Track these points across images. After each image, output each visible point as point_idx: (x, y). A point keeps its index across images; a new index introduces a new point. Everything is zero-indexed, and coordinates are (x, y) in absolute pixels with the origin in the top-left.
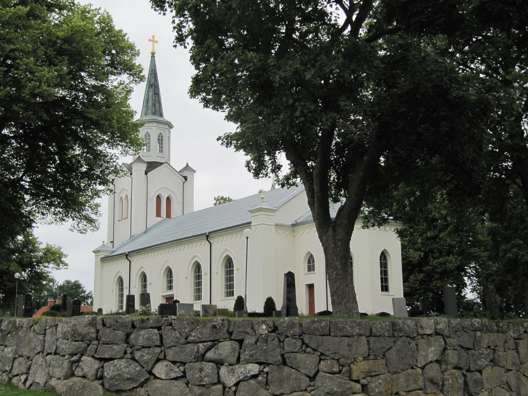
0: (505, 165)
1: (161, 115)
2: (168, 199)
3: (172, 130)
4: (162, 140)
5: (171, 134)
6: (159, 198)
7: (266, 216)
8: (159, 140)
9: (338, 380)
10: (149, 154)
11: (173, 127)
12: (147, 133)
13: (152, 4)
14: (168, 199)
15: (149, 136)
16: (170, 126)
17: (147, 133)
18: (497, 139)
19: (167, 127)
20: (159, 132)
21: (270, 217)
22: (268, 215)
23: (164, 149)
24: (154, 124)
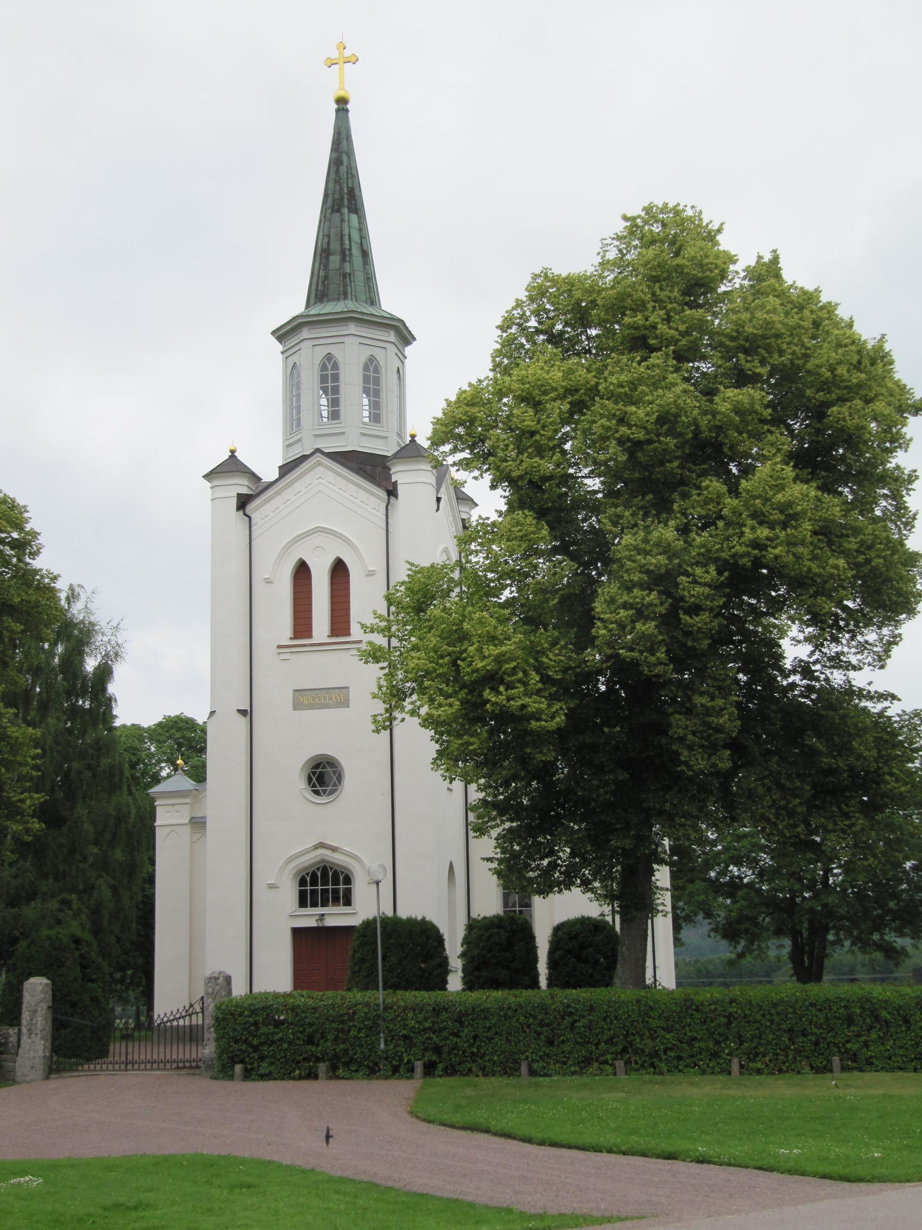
0: (745, 826)
1: (373, 300)
2: (339, 570)
3: (408, 350)
4: (336, 378)
5: (406, 361)
6: (302, 572)
7: (169, 808)
8: (323, 379)
9: (779, 459)
10: (335, 427)
11: (414, 339)
12: (329, 357)
13: (701, 220)
14: (339, 570)
15: (336, 366)
16: (404, 336)
17: (329, 357)
18: (842, 890)
19: (392, 336)
20: (365, 353)
21: (177, 808)
22: (173, 805)
23: (384, 411)
24: (352, 328)
